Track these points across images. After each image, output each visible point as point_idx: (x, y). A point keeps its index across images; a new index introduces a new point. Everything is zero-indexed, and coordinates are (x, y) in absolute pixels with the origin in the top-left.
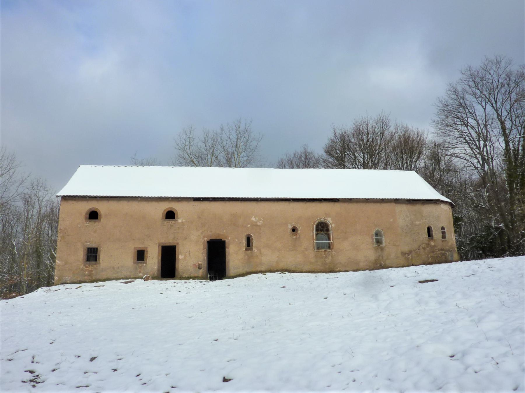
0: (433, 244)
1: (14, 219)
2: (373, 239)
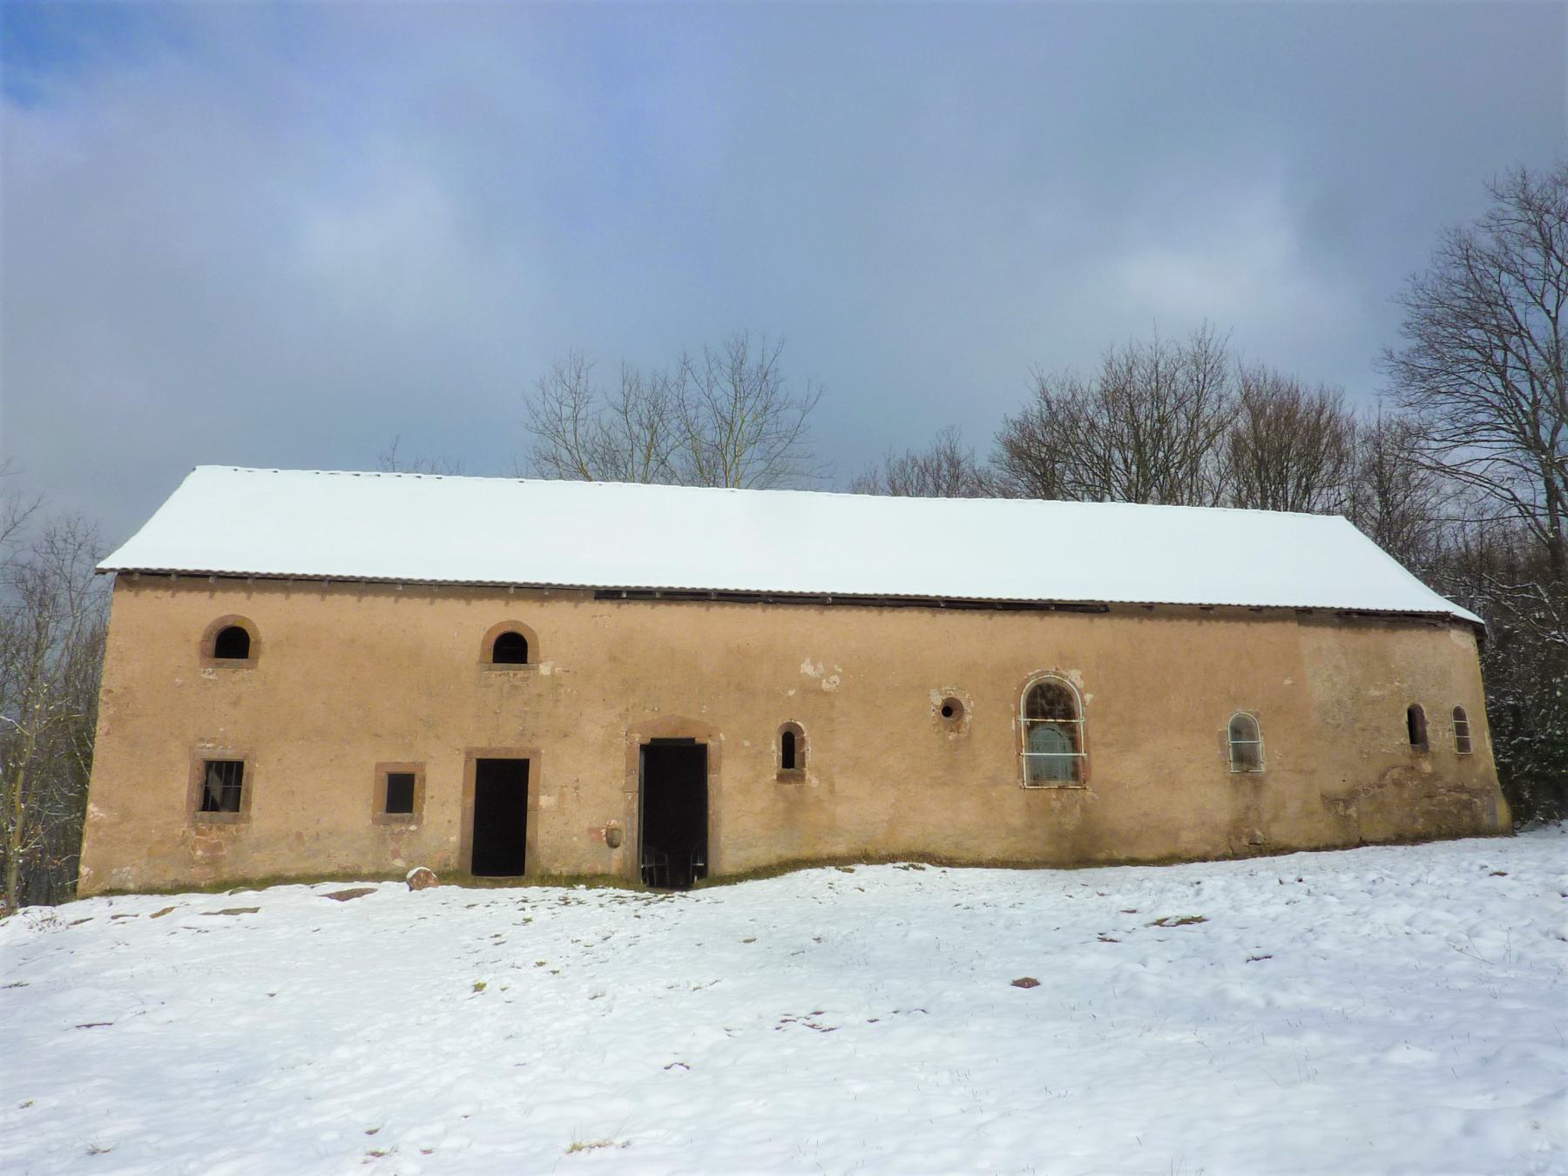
2: (1223, 747)
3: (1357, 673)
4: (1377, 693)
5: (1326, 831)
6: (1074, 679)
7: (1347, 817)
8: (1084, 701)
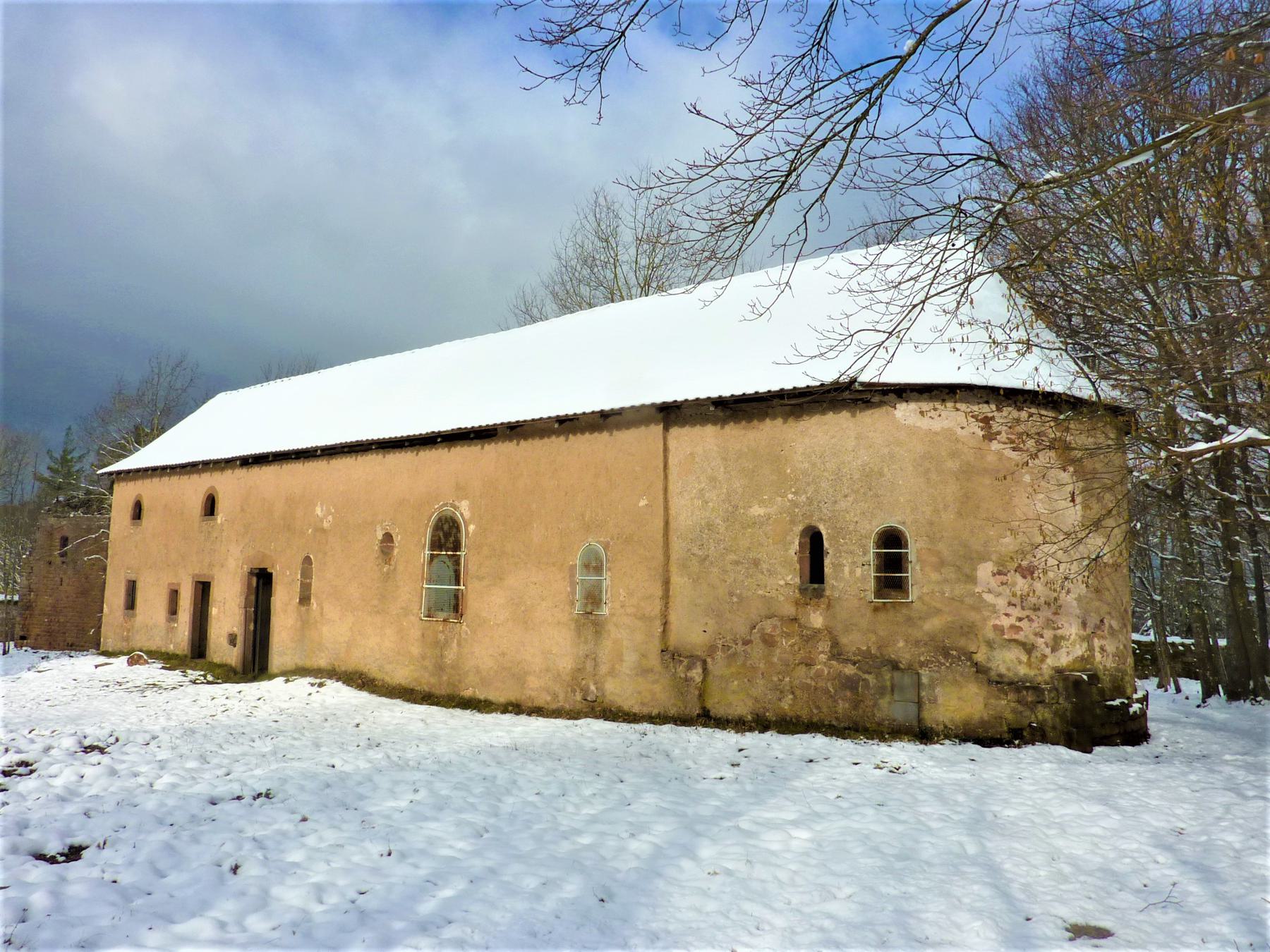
0: (817, 620)
2: (573, 584)
3: (737, 485)
6: (464, 510)
7: (687, 680)
8: (469, 531)
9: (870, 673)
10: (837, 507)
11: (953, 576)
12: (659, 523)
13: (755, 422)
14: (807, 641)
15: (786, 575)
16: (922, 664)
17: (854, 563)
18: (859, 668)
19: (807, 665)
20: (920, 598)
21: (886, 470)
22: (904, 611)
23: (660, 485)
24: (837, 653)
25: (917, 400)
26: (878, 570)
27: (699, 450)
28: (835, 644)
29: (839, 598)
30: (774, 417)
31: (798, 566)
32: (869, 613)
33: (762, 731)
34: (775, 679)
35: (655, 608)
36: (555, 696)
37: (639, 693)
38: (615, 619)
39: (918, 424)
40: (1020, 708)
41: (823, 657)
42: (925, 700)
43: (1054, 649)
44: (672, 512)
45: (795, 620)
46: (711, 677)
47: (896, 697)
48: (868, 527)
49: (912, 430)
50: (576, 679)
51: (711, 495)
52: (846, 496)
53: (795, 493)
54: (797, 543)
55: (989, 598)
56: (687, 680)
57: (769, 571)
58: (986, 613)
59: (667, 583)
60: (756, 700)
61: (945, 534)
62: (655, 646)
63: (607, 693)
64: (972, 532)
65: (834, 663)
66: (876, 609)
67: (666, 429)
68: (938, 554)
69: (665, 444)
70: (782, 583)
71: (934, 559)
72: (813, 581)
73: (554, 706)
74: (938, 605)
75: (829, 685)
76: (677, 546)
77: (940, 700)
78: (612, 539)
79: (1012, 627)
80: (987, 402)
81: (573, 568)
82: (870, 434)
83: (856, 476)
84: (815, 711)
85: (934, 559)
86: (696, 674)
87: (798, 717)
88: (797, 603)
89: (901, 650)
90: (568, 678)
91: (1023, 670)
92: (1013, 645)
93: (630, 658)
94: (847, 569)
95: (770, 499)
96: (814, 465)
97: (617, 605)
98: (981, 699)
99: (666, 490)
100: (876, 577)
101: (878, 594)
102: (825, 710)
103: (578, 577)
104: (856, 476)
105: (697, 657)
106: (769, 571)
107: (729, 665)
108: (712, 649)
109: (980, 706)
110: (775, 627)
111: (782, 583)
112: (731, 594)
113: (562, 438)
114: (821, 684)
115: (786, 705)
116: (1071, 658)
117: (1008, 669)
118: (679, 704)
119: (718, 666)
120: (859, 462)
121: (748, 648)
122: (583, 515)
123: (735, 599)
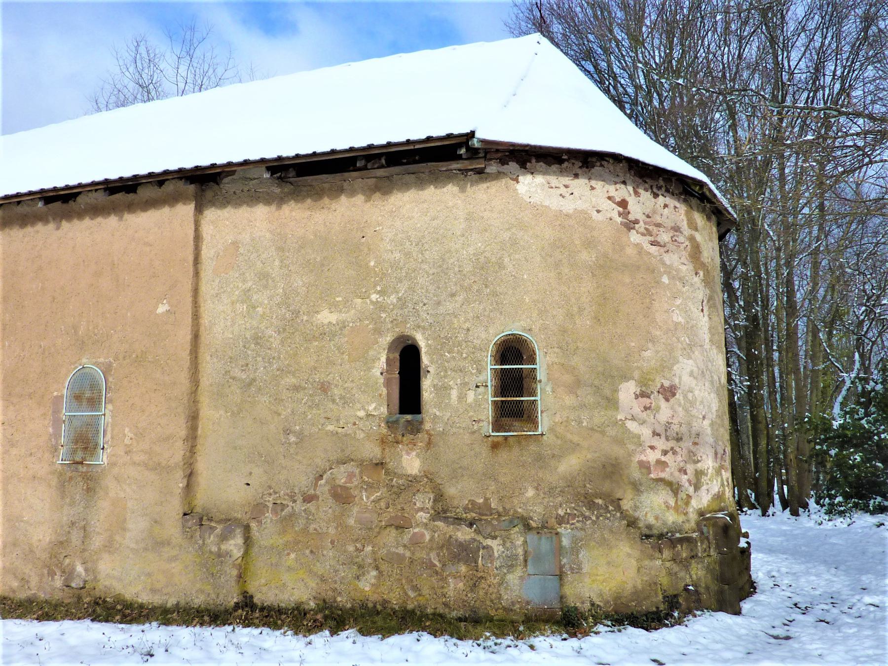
0: (411, 463)
1: (756, 135)
2: (57, 422)
3: (298, 282)
4: (333, 318)
5: (184, 583)
9: (495, 538)
10: (441, 309)
11: (591, 399)
12: (184, 335)
13: (326, 200)
14: (398, 495)
15: (375, 401)
16: (561, 520)
17: (465, 384)
18: (477, 532)
19: (397, 527)
20: (552, 430)
21: (506, 260)
22: (533, 447)
23: (188, 286)
24: (442, 512)
25: (545, 173)
26: (496, 395)
27: (246, 237)
28: (439, 497)
29: (443, 433)
30: (352, 193)
31: (384, 391)
32: (484, 451)
33: (334, 632)
34: (351, 548)
35: (177, 453)
36: (24, 581)
37: (149, 575)
38: (116, 470)
39: (547, 203)
40: (676, 568)
41: (422, 516)
42: (566, 569)
43: (697, 488)
44: (205, 320)
45: (381, 464)
46: (255, 550)
47: (530, 569)
48: (483, 335)
49: (539, 211)
50: (56, 557)
51: (260, 297)
52: (453, 295)
53: (381, 293)
54: (383, 359)
55: (632, 426)
56: (219, 555)
57: (342, 397)
58: (631, 447)
59: (193, 418)
60: (323, 579)
61: (580, 345)
62: (175, 507)
63: (101, 576)
64: (611, 342)
65: (440, 524)
66: (495, 446)
67: (199, 210)
68: (572, 370)
69: (197, 230)
70: (361, 414)
71: (568, 378)
72: (403, 410)
73: (22, 595)
74: (576, 439)
75: (433, 555)
76: (210, 369)
77: (586, 568)
78: (116, 359)
79: (659, 462)
80: (624, 183)
81: (58, 400)
82: (486, 214)
83: (468, 268)
84: (412, 594)
85: (568, 378)
86: (234, 546)
87: (385, 602)
88: (383, 441)
89: (531, 501)
90: (45, 556)
91: (671, 518)
92: (661, 486)
93: (137, 526)
94: (454, 394)
95: (346, 301)
96: (408, 255)
97: (121, 451)
98: (634, 562)
99: (196, 291)
100: (494, 402)
101: (498, 426)
102: (426, 591)
103: (64, 413)
104: (468, 268)
105: (237, 522)
106: (342, 397)
107: (284, 532)
108: (258, 509)
109: (632, 573)
110: (351, 476)
111: (361, 414)
112: (287, 432)
113: (51, 226)
114: (421, 554)
115: (367, 586)
116: (709, 497)
117: (657, 518)
118: (208, 588)
119: (267, 533)
120: (471, 250)
121: (311, 506)
122: (75, 328)
123: (293, 439)
